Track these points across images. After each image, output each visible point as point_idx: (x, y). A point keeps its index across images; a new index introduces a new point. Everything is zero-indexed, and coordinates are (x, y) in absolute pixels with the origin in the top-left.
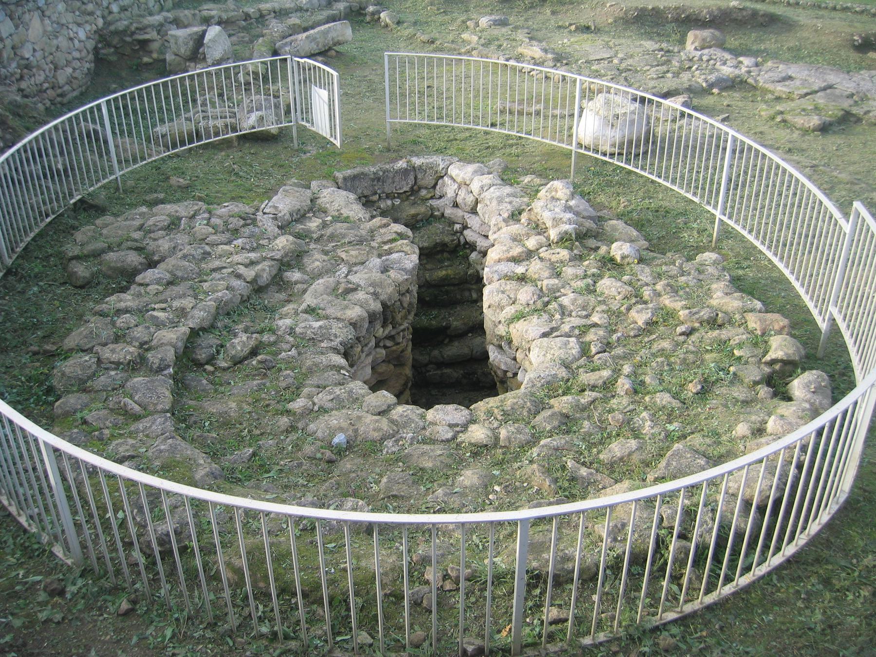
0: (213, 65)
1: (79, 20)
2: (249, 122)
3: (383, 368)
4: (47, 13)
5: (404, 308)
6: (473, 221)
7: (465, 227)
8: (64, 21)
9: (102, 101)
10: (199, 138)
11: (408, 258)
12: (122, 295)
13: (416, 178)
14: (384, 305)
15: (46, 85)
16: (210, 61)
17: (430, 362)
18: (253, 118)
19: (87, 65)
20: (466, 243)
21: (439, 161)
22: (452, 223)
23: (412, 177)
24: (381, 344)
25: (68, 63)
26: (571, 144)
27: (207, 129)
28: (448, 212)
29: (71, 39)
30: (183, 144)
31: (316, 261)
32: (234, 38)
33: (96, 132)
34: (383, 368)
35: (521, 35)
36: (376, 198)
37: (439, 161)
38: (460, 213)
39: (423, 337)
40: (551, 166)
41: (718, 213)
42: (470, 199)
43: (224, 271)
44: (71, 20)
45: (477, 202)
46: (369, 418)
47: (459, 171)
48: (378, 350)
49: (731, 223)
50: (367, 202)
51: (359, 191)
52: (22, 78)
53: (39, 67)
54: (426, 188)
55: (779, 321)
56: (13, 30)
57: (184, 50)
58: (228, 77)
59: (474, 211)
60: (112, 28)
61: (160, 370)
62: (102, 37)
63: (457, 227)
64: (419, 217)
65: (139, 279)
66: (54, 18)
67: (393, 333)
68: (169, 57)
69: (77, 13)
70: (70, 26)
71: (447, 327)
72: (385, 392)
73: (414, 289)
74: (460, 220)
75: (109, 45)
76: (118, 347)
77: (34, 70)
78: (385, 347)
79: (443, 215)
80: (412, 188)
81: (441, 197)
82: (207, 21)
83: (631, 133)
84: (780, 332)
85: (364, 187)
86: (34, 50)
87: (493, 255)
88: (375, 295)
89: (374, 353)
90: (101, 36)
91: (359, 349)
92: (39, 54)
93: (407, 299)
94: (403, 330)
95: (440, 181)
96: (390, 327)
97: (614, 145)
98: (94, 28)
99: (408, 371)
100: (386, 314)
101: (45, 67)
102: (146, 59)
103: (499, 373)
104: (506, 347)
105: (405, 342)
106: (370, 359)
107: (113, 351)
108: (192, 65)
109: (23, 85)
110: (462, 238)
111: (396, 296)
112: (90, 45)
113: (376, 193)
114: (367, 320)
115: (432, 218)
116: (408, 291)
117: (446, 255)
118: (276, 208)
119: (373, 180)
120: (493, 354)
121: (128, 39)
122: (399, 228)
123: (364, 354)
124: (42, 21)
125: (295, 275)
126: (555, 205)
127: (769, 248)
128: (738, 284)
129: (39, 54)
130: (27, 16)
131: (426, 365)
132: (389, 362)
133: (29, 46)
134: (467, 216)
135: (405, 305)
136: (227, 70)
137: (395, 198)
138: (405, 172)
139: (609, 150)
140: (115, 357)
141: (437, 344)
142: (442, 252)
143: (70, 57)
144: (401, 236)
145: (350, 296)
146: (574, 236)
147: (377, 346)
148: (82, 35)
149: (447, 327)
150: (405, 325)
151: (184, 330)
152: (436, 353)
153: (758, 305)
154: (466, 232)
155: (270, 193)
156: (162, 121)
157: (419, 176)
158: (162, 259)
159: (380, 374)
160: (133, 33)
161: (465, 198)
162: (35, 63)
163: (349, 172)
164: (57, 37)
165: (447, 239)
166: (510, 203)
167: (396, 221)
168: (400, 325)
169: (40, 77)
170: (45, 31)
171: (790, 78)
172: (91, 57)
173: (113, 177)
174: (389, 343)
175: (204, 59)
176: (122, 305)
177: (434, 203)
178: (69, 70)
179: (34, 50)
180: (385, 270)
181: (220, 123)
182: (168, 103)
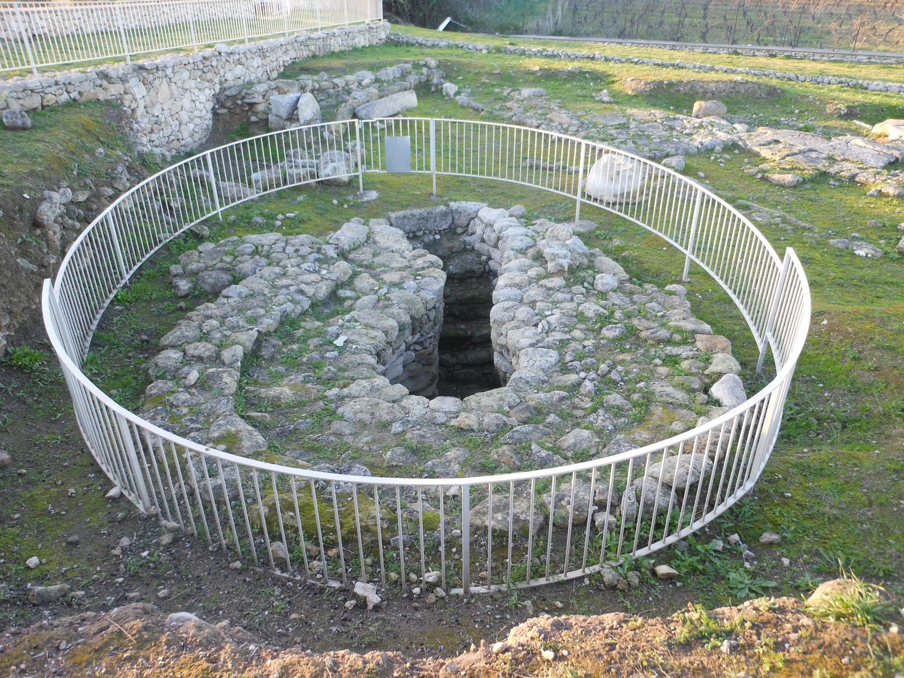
0: (304, 124)
1: (200, 86)
2: (326, 173)
3: (413, 367)
4: (173, 80)
5: (430, 321)
6: (495, 254)
7: (490, 258)
8: (187, 86)
9: (208, 152)
10: (285, 183)
11: (435, 282)
12: (210, 305)
13: (453, 219)
14: (412, 318)
15: (172, 138)
16: (302, 121)
17: (457, 364)
18: (328, 170)
19: (207, 122)
20: (490, 271)
21: (470, 206)
22: (479, 254)
23: (450, 218)
24: (412, 348)
25: (191, 120)
26: (575, 193)
27: (291, 176)
28: (477, 246)
29: (193, 101)
30: (271, 187)
31: (364, 281)
32: (324, 103)
33: (202, 177)
34: (413, 367)
35: (554, 105)
36: (421, 233)
37: (470, 206)
38: (485, 247)
39: (447, 343)
40: (561, 212)
41: (688, 253)
42: (493, 236)
43: (291, 288)
44: (194, 86)
45: (499, 239)
46: (385, 405)
47: (487, 213)
48: (409, 352)
49: (698, 261)
50: (412, 237)
51: (408, 228)
52: (152, 131)
53: (167, 123)
54: (461, 227)
55: (722, 341)
56: (145, 92)
57: (284, 113)
58: (315, 134)
59: (496, 246)
60: (228, 93)
61: (231, 365)
62: (219, 100)
63: (484, 258)
64: (454, 250)
65: (224, 292)
66: (179, 84)
67: (422, 340)
68: (271, 118)
69: (199, 80)
70: (192, 91)
71: (472, 336)
72: (400, 385)
73: (441, 306)
74: (486, 253)
75: (223, 106)
76: (201, 345)
77: (163, 125)
78: (415, 350)
79: (473, 248)
80: (450, 226)
81: (472, 234)
82: (303, 89)
83: (629, 187)
84: (723, 350)
85: (411, 225)
86: (163, 110)
87: (501, 281)
88: (408, 310)
89: (405, 354)
90: (217, 99)
91: (391, 351)
92: (166, 112)
93: (432, 315)
94: (430, 338)
95: (472, 222)
96: (418, 335)
97: (615, 196)
98: (213, 92)
99: (434, 369)
100: (416, 325)
101: (172, 123)
102: (253, 119)
103: (501, 374)
104: (505, 354)
105: (432, 346)
106: (401, 359)
107: (196, 348)
108: (289, 123)
109: (154, 137)
110: (487, 267)
111: (423, 311)
112: (209, 106)
113: (421, 230)
114: (397, 329)
115: (467, 249)
116: (434, 308)
117: (474, 280)
118: (338, 239)
119: (419, 220)
120: (497, 359)
121: (239, 102)
122: (434, 258)
123: (396, 356)
124: (169, 85)
125: (345, 293)
126: (561, 242)
127: (726, 282)
128: (697, 311)
129: (166, 112)
130: (157, 82)
131: (453, 366)
132: (419, 362)
133: (159, 106)
134: (491, 249)
135: (432, 318)
136: (315, 129)
137: (436, 234)
138: (444, 215)
139: (612, 200)
140: (196, 353)
141: (456, 350)
142: (471, 277)
143: (192, 115)
144: (432, 264)
145: (386, 310)
146: (566, 268)
147: (408, 349)
148: (203, 98)
149: (472, 336)
150: (432, 334)
151: (254, 333)
152: (462, 356)
153: (707, 327)
154: (490, 262)
155: (337, 226)
156: (255, 170)
157: (456, 217)
158: (245, 276)
159: (411, 371)
160: (244, 98)
161: (491, 236)
162: (163, 120)
163: (401, 213)
164: (182, 99)
165: (475, 267)
166: (521, 240)
167: (434, 253)
168: (427, 334)
169: (167, 131)
170: (172, 95)
171: (777, 142)
172: (210, 115)
173: (215, 212)
174: (418, 348)
175: (298, 120)
176: (209, 312)
177: (468, 239)
178: (191, 126)
179: (163, 110)
180: (418, 290)
181: (302, 171)
182: (453, 144)
